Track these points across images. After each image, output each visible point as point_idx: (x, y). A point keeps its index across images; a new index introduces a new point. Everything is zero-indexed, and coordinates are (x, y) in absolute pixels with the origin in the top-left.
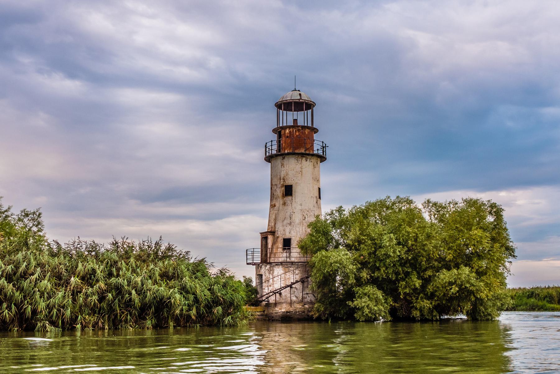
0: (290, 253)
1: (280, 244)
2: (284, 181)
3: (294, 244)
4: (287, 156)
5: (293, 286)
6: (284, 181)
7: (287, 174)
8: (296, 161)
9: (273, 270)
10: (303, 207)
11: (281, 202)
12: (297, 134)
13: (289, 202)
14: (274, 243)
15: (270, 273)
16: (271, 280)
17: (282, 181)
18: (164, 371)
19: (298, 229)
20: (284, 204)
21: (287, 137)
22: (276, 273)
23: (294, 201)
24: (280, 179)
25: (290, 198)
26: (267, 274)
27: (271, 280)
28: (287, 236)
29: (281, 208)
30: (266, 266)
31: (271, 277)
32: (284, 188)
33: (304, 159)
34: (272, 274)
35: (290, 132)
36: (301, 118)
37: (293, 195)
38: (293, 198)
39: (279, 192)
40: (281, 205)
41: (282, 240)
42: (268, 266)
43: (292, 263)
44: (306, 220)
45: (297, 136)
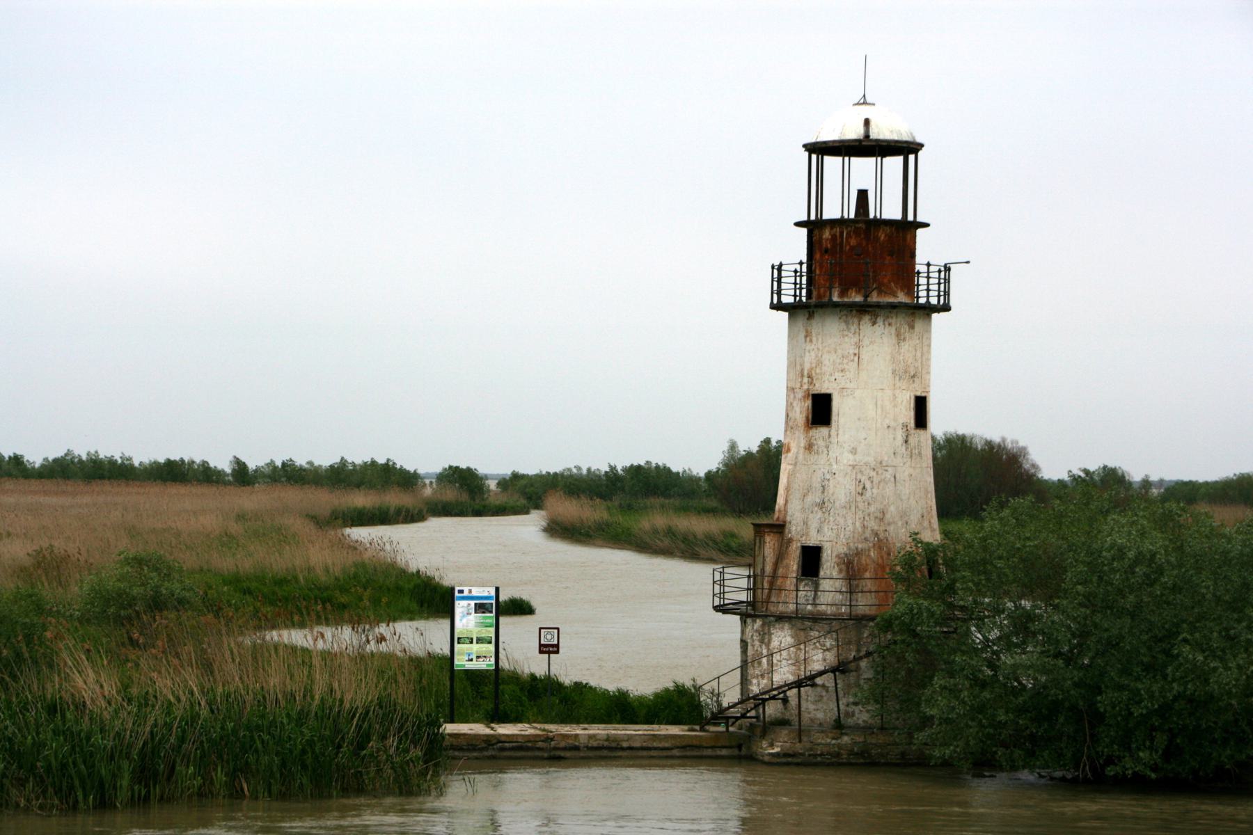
0: (816, 590)
1: (793, 563)
2: (811, 383)
3: (829, 566)
4: (820, 311)
5: (819, 681)
6: (811, 383)
7: (819, 363)
8: (843, 326)
9: (770, 634)
10: (858, 457)
11: (803, 443)
12: (853, 242)
13: (821, 443)
14: (780, 557)
15: (762, 641)
16: (764, 660)
17: (806, 380)
18: (477, 758)
19: (842, 521)
20: (810, 447)
21: (826, 251)
22: (775, 643)
23: (834, 440)
24: (802, 376)
25: (823, 431)
26: (757, 643)
27: (764, 660)
28: (812, 541)
29: (801, 457)
30: (754, 621)
31: (765, 652)
32: (809, 403)
33: (866, 318)
34: (768, 645)
35: (834, 237)
36: (881, 182)
37: (833, 423)
38: (833, 432)
39: (802, 409)
40: (802, 450)
41: (798, 552)
42: (759, 622)
43: (816, 619)
44: (868, 494)
45: (852, 248)
